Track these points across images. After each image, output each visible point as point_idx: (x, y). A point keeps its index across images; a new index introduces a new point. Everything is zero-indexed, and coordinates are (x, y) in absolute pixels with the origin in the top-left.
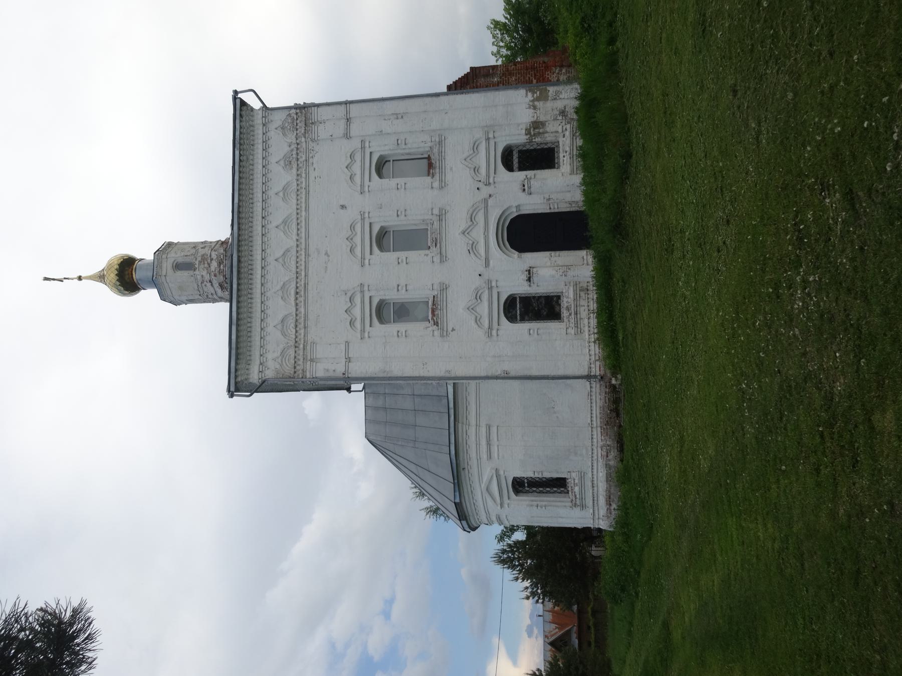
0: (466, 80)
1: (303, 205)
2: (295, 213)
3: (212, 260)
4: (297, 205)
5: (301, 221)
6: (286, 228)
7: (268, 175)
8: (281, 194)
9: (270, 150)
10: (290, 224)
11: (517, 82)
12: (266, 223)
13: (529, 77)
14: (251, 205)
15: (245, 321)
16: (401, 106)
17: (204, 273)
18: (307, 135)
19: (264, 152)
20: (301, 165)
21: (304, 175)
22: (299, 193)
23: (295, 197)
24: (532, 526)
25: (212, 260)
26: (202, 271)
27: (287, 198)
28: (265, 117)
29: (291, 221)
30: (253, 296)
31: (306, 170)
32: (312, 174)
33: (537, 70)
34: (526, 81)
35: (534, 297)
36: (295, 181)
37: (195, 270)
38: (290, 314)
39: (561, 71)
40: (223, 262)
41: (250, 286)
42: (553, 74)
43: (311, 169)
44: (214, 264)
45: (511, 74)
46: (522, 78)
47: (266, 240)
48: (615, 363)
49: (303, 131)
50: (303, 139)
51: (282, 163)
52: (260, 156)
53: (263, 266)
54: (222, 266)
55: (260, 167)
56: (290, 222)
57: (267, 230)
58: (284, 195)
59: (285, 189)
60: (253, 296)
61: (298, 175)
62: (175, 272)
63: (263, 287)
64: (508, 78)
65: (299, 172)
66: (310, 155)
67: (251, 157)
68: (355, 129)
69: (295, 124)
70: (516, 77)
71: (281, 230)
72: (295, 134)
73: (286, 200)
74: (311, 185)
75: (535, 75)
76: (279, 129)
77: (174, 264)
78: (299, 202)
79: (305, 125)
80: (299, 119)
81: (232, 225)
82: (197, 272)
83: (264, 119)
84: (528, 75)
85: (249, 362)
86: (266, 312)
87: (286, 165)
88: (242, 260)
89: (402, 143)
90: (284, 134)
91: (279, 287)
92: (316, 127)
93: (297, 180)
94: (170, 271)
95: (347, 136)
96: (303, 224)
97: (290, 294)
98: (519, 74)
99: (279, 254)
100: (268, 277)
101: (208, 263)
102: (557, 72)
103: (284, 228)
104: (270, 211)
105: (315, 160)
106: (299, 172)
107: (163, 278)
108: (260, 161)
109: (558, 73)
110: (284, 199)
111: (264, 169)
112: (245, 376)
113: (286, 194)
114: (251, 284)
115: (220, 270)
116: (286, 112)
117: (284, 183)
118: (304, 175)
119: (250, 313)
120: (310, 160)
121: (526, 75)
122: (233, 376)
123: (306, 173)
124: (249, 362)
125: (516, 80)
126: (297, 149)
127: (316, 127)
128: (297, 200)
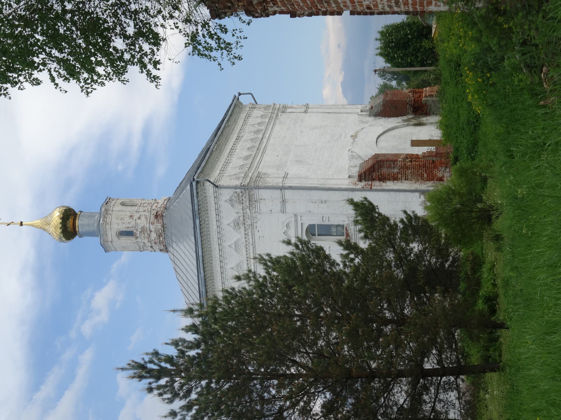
0: (372, 170)
2: (245, 260)
3: (151, 231)
4: (247, 254)
6: (239, 268)
9: (222, 215)
11: (412, 174)
12: (223, 265)
13: (421, 172)
16: (325, 195)
17: (146, 241)
18: (251, 208)
19: (217, 216)
20: (247, 227)
21: (250, 234)
22: (247, 246)
23: (244, 248)
24: (399, 154)
25: (151, 231)
26: (143, 238)
27: (238, 249)
28: (216, 192)
31: (252, 232)
32: (257, 235)
33: (428, 168)
34: (419, 174)
36: (244, 239)
37: (137, 238)
39: (446, 170)
40: (162, 236)
42: (440, 171)
43: (256, 231)
44: (153, 236)
45: (407, 168)
46: (416, 172)
47: (224, 276)
48: (493, 169)
49: (248, 204)
50: (248, 210)
51: (232, 225)
52: (214, 219)
54: (161, 238)
55: (215, 227)
57: (224, 269)
58: (235, 246)
59: (236, 243)
61: (245, 234)
62: (119, 239)
64: (405, 170)
65: (246, 232)
66: (254, 221)
67: (207, 219)
68: (289, 207)
69: (241, 200)
70: (411, 170)
71: (235, 270)
72: (242, 207)
73: (238, 250)
74: (256, 240)
75: (426, 171)
76: (228, 201)
77: (118, 233)
78: (248, 253)
79: (249, 201)
80: (244, 195)
82: (139, 240)
83: (215, 193)
84: (421, 171)
87: (235, 226)
89: (326, 220)
90: (233, 206)
92: (258, 203)
93: (245, 238)
94: (115, 238)
95: (283, 211)
98: (414, 169)
101: (148, 234)
102: (442, 170)
103: (237, 268)
104: (225, 256)
105: (258, 225)
106: (246, 232)
107: (110, 244)
108: (215, 223)
109: (443, 171)
110: (236, 250)
113: (237, 246)
115: (160, 241)
116: (234, 190)
117: (235, 239)
118: (250, 234)
120: (254, 224)
121: (419, 170)
123: (252, 234)
125: (411, 172)
126: (244, 216)
127: (258, 203)
128: (247, 251)
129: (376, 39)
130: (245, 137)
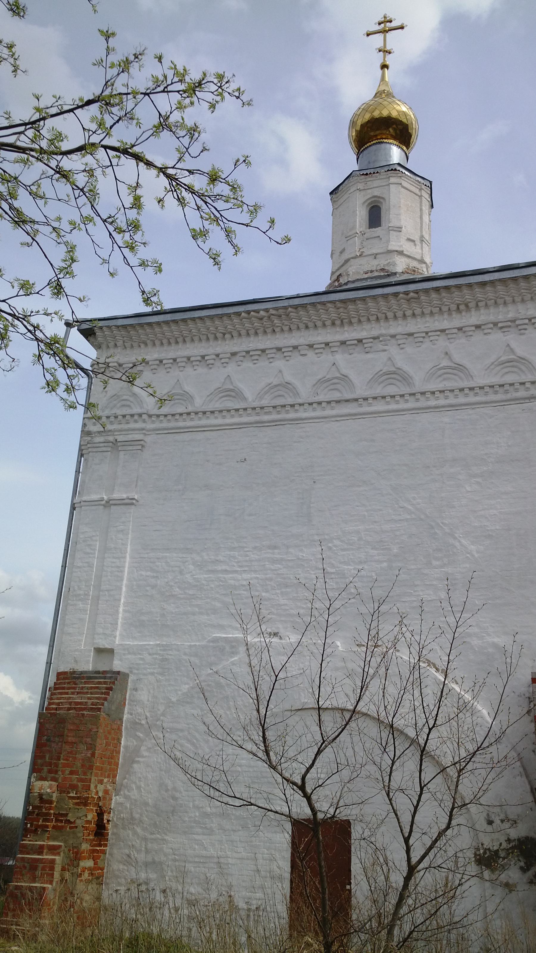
1: (266, 418)
5: (397, 402)
7: (218, 363)
8: (445, 363)
10: (181, 401)
14: (286, 328)
15: (479, 296)
29: (461, 378)
30: (473, 310)
35: (37, 741)
38: (297, 394)
41: (196, 338)
53: (251, 353)
56: (520, 369)
60: (473, 310)
63: (473, 328)
77: (381, 200)
81: (298, 297)
85: (142, 346)
86: (427, 340)
88: (488, 288)
91: (457, 358)
96: (393, 406)
97: (445, 379)
99: (401, 362)
100: (478, 336)
111: (185, 359)
112: (529, 296)
114: (192, 340)
119: (360, 321)
122: (297, 302)
124: (227, 336)
127: (109, 449)
129: (94, 94)
130: (369, 356)
